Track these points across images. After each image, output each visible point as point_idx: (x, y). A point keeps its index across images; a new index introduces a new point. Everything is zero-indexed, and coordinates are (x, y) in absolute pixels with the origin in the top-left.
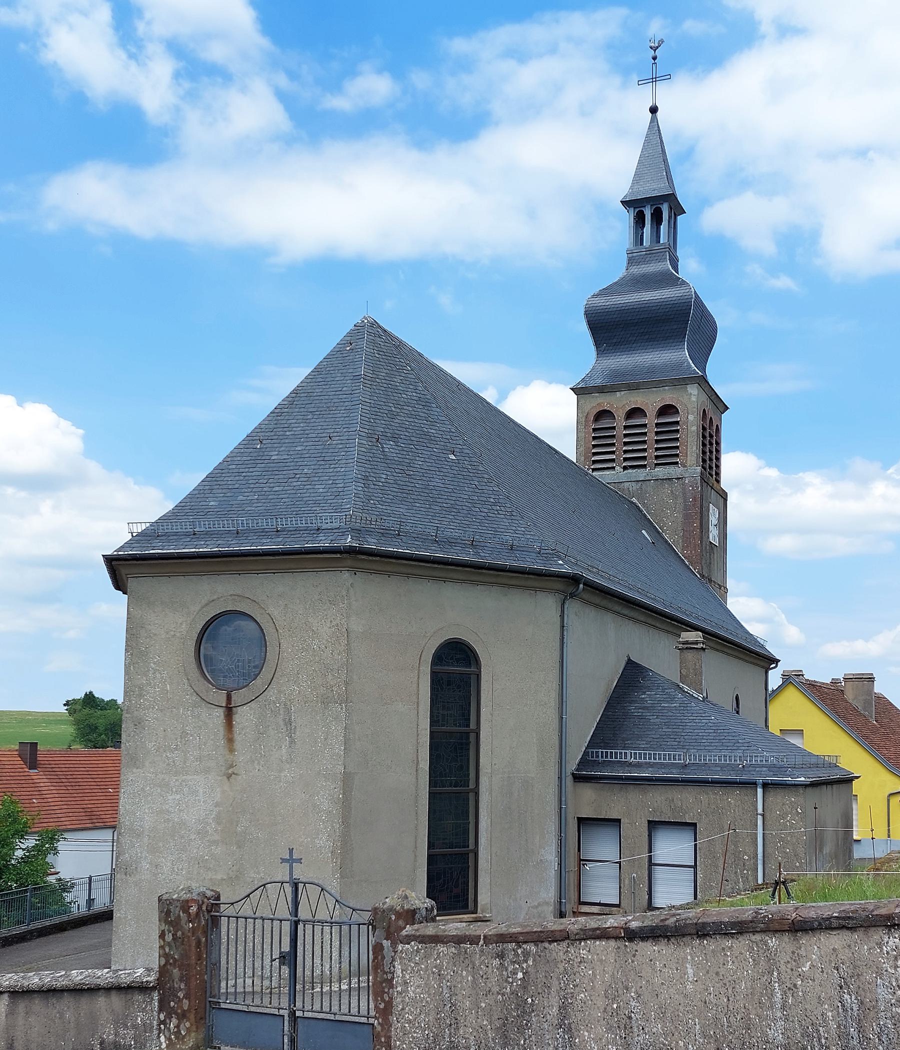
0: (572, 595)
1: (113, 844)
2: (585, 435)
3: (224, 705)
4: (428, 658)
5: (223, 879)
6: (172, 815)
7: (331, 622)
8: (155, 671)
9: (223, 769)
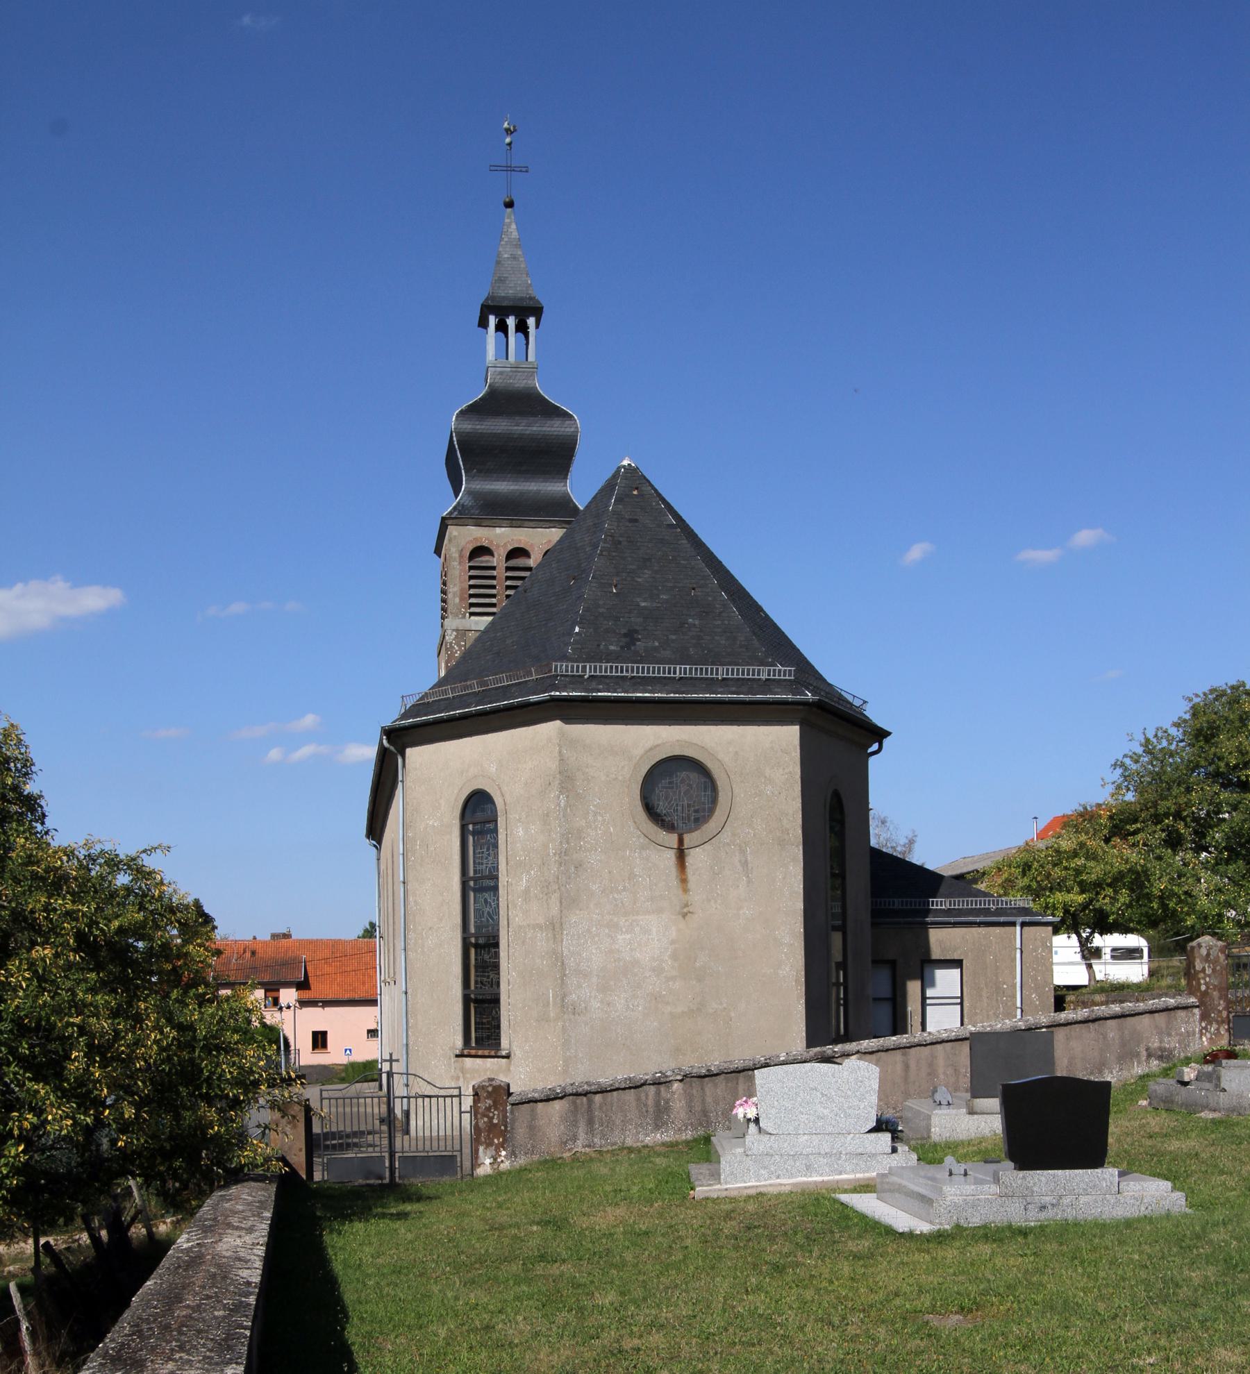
2: (460, 573)
3: (676, 846)
5: (683, 1012)
8: (595, 814)
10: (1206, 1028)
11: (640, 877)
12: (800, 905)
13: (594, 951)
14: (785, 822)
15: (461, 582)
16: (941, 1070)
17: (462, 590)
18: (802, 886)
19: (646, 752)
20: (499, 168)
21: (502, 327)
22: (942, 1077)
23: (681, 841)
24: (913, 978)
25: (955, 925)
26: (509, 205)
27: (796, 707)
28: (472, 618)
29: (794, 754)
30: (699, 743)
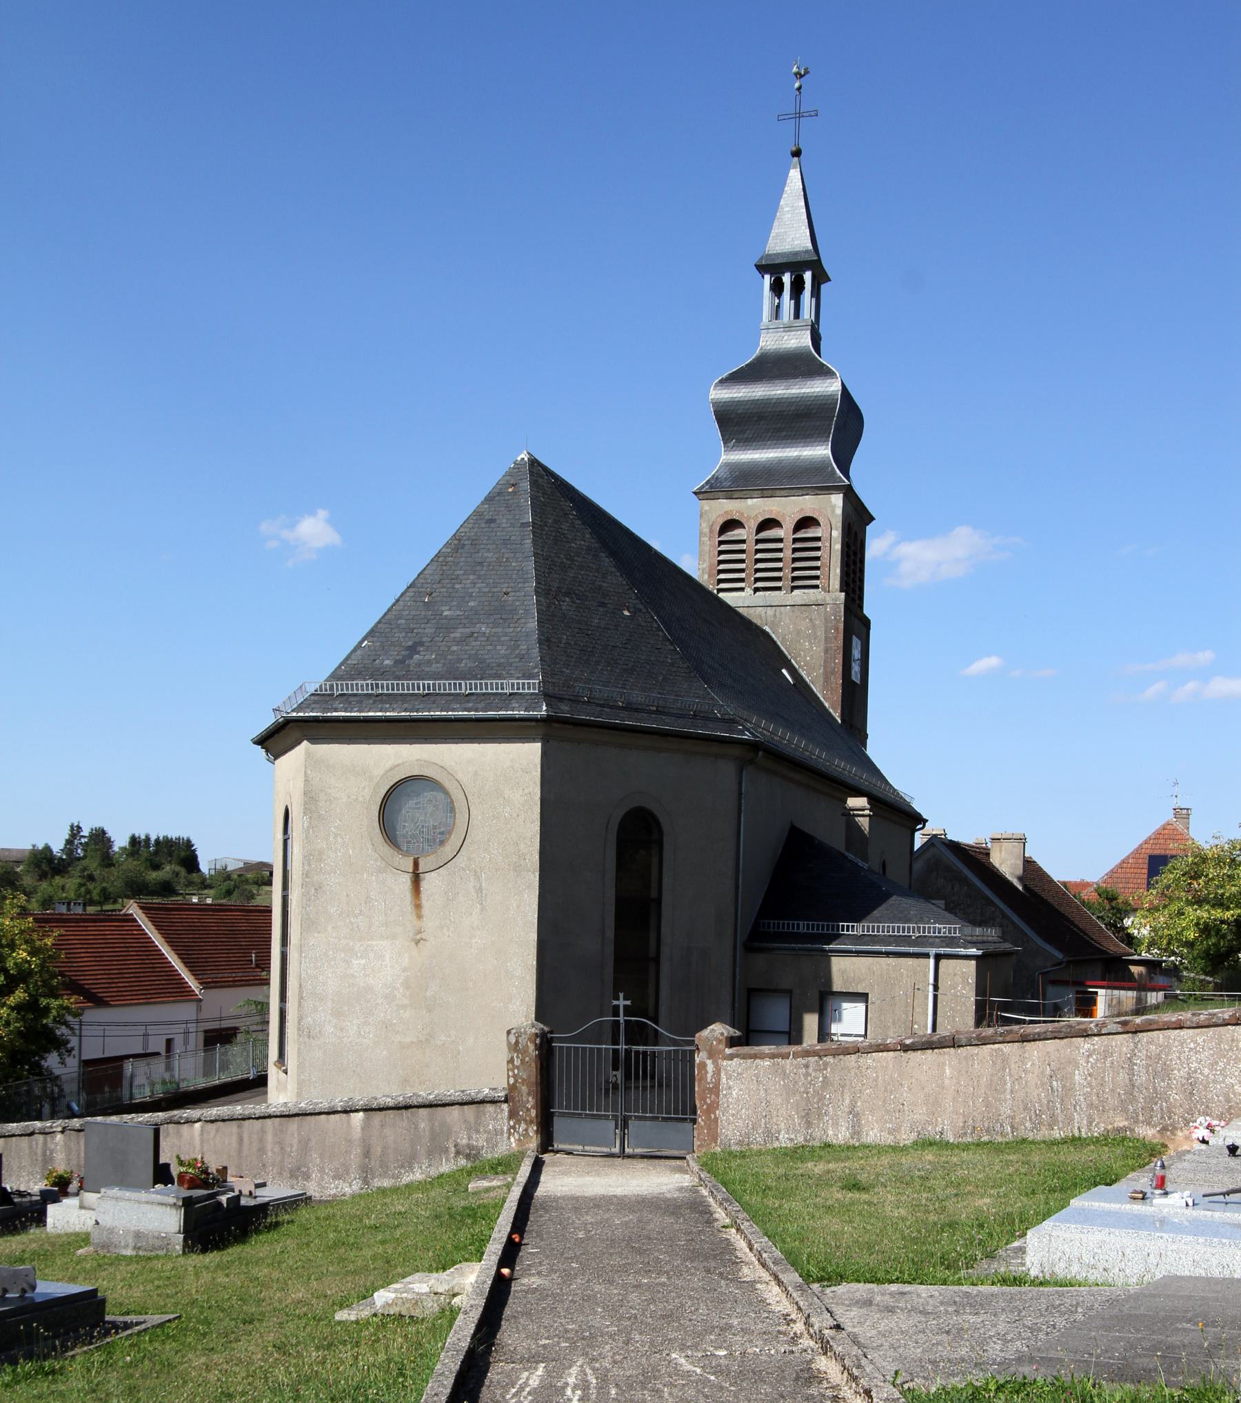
0: (751, 762)
1: (81, 1033)
3: (411, 870)
4: (614, 827)
5: (412, 1043)
6: (358, 980)
7: (523, 790)
8: (336, 836)
9: (411, 934)
10: (514, 1127)
11: (376, 901)
12: (534, 936)
13: (330, 975)
14: (522, 846)
15: (710, 558)
16: (269, 1147)
17: (711, 566)
18: (536, 916)
19: (387, 772)
20: (786, 117)
21: (777, 288)
22: (270, 1154)
23: (416, 864)
24: (811, 1011)
25: (859, 953)
26: (797, 153)
27: (528, 724)
28: (758, 593)
29: (534, 773)
30: (439, 763)
